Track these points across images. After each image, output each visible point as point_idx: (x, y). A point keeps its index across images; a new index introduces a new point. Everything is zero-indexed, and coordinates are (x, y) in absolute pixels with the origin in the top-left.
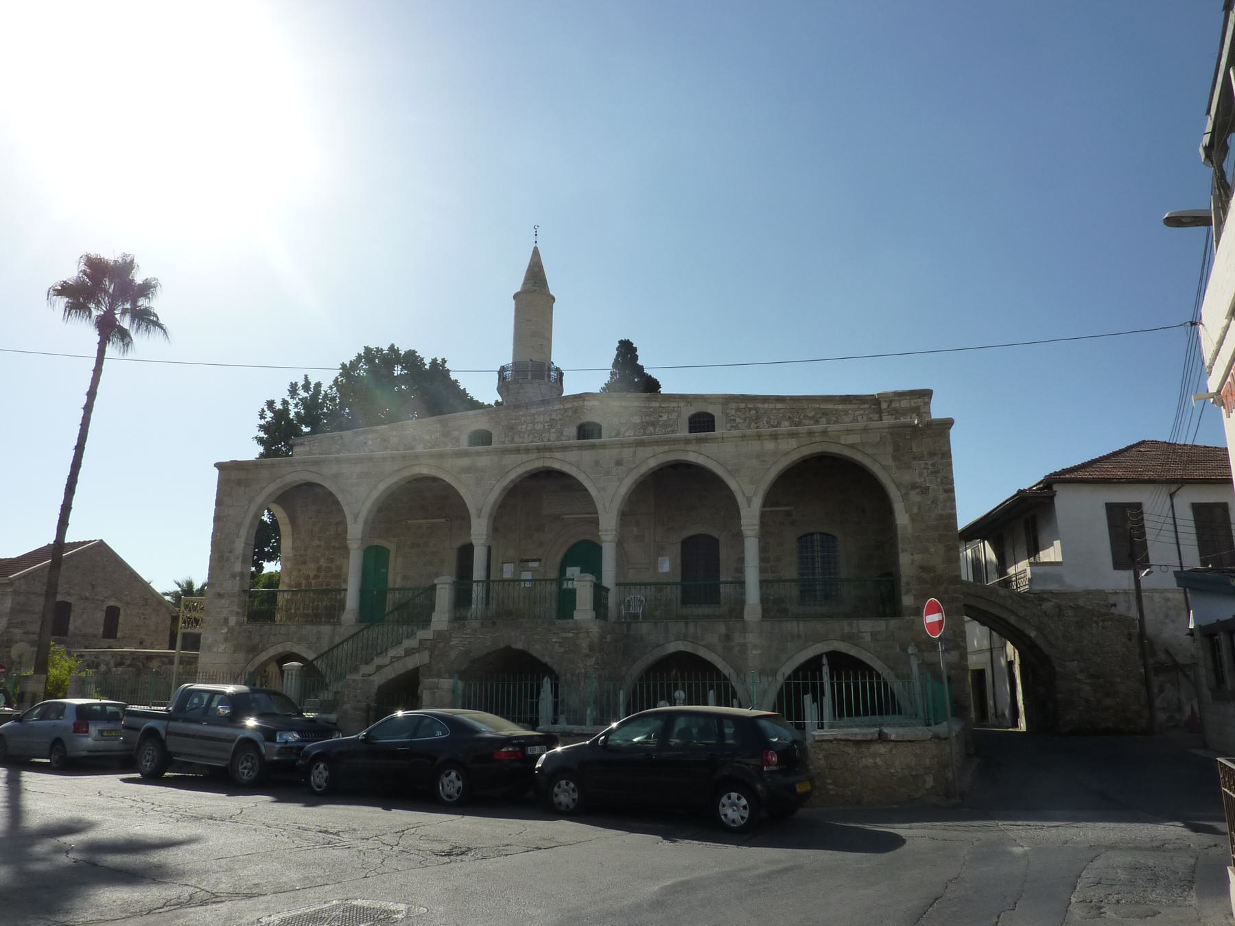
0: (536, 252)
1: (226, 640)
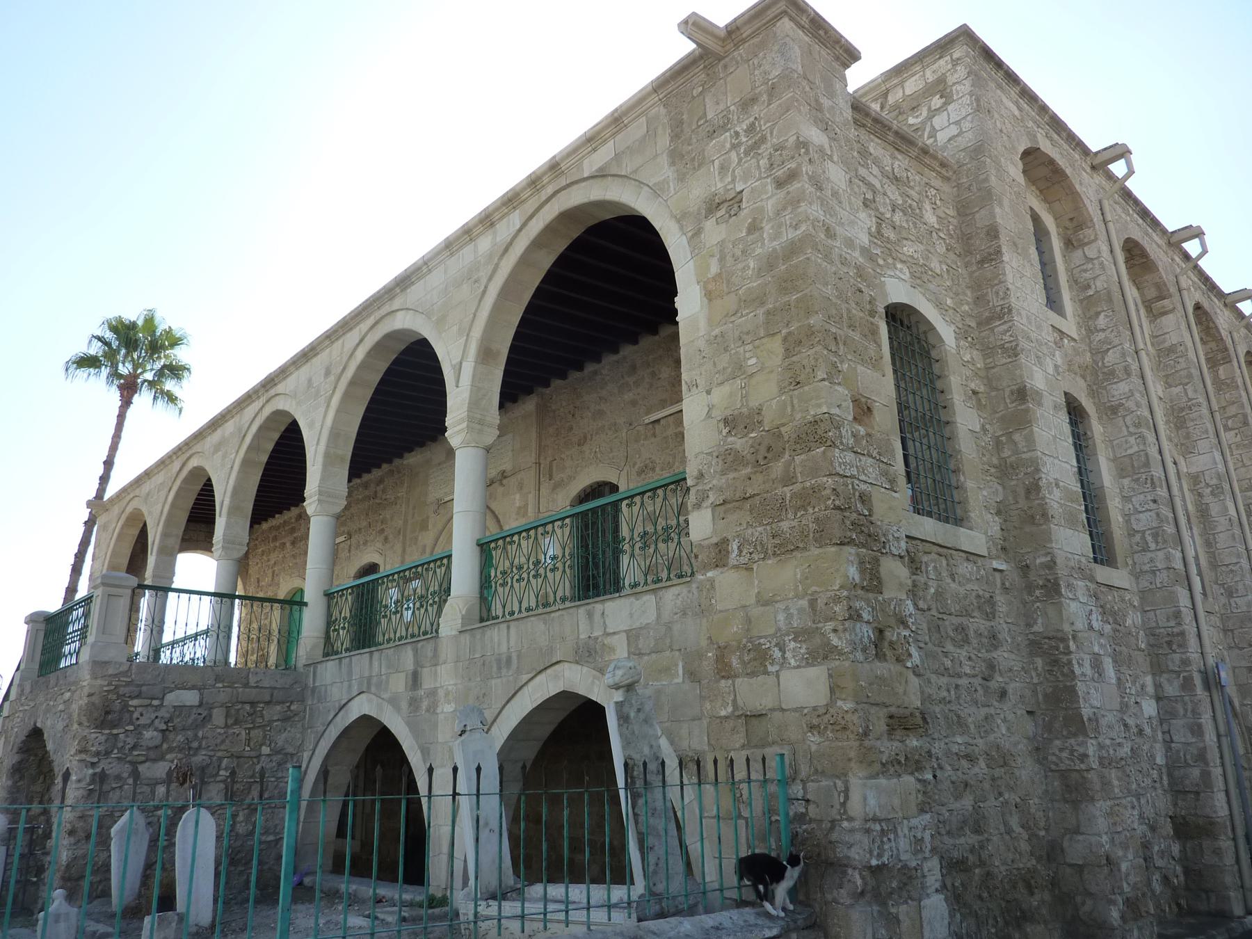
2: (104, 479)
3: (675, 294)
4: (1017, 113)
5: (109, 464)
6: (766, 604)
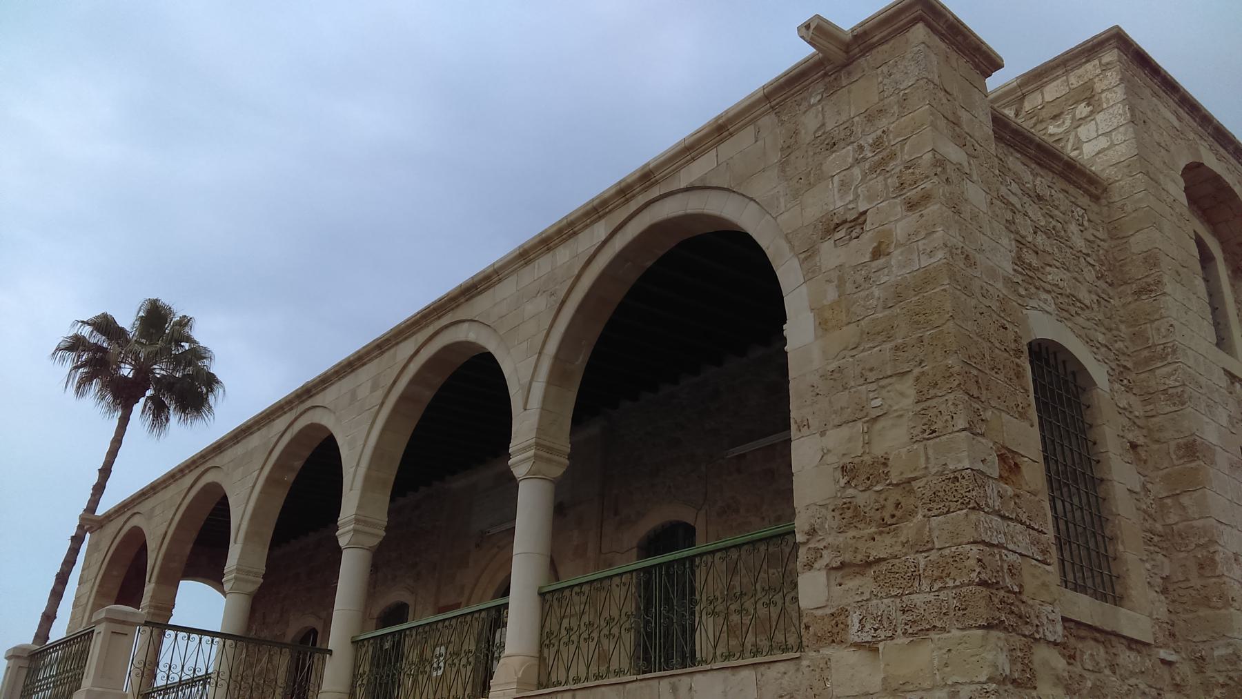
2: (99, 489)
3: (784, 320)
4: (1176, 123)
5: (105, 472)
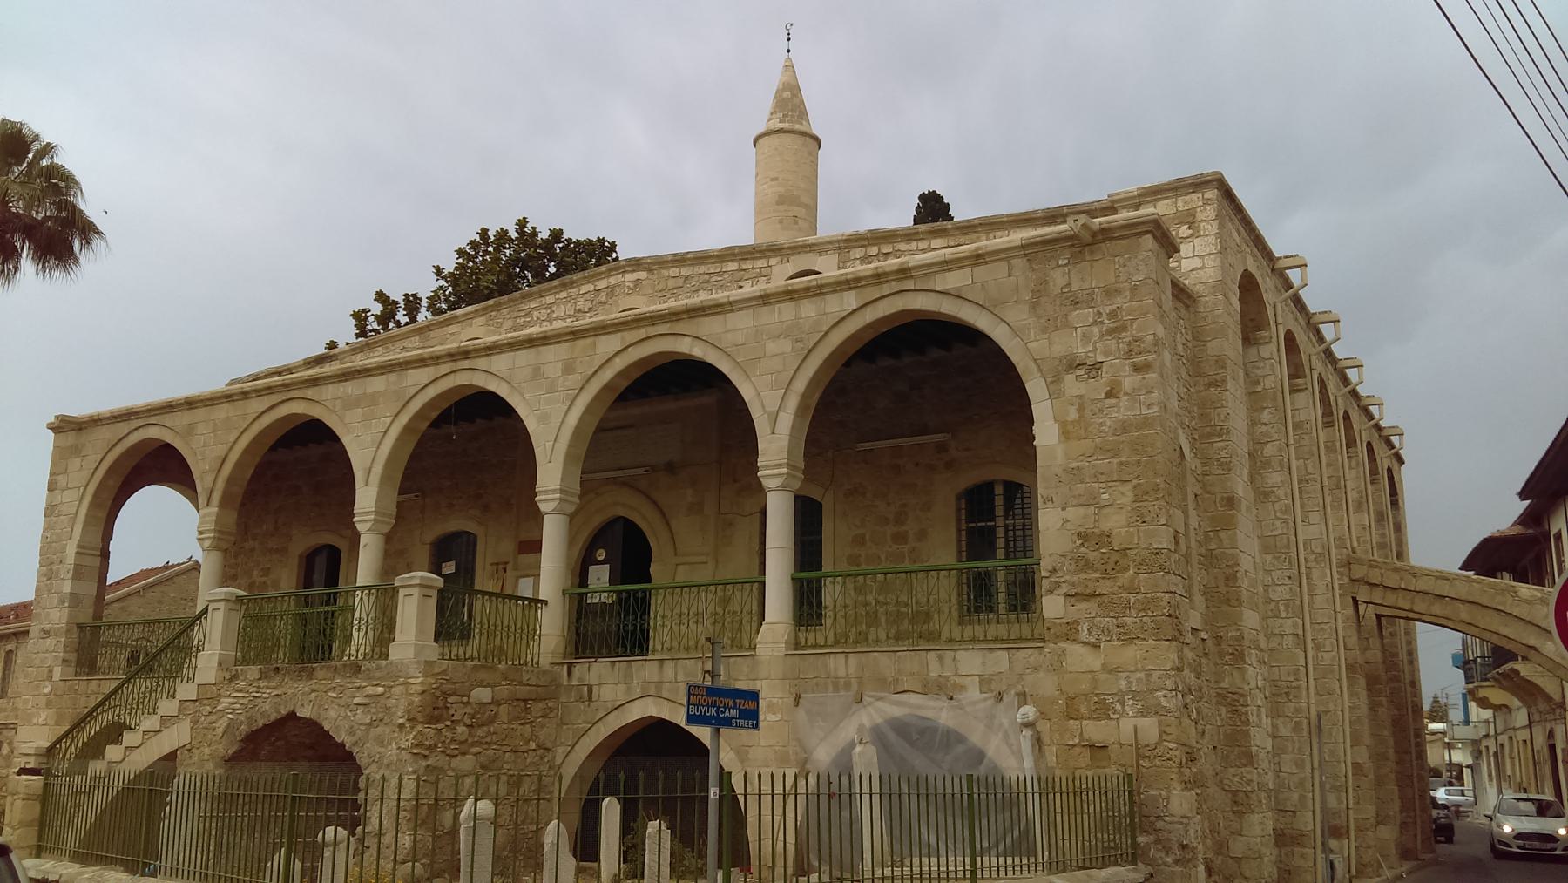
0: (789, 67)
1: (49, 704)
3: (1032, 422)
6: (1110, 672)
